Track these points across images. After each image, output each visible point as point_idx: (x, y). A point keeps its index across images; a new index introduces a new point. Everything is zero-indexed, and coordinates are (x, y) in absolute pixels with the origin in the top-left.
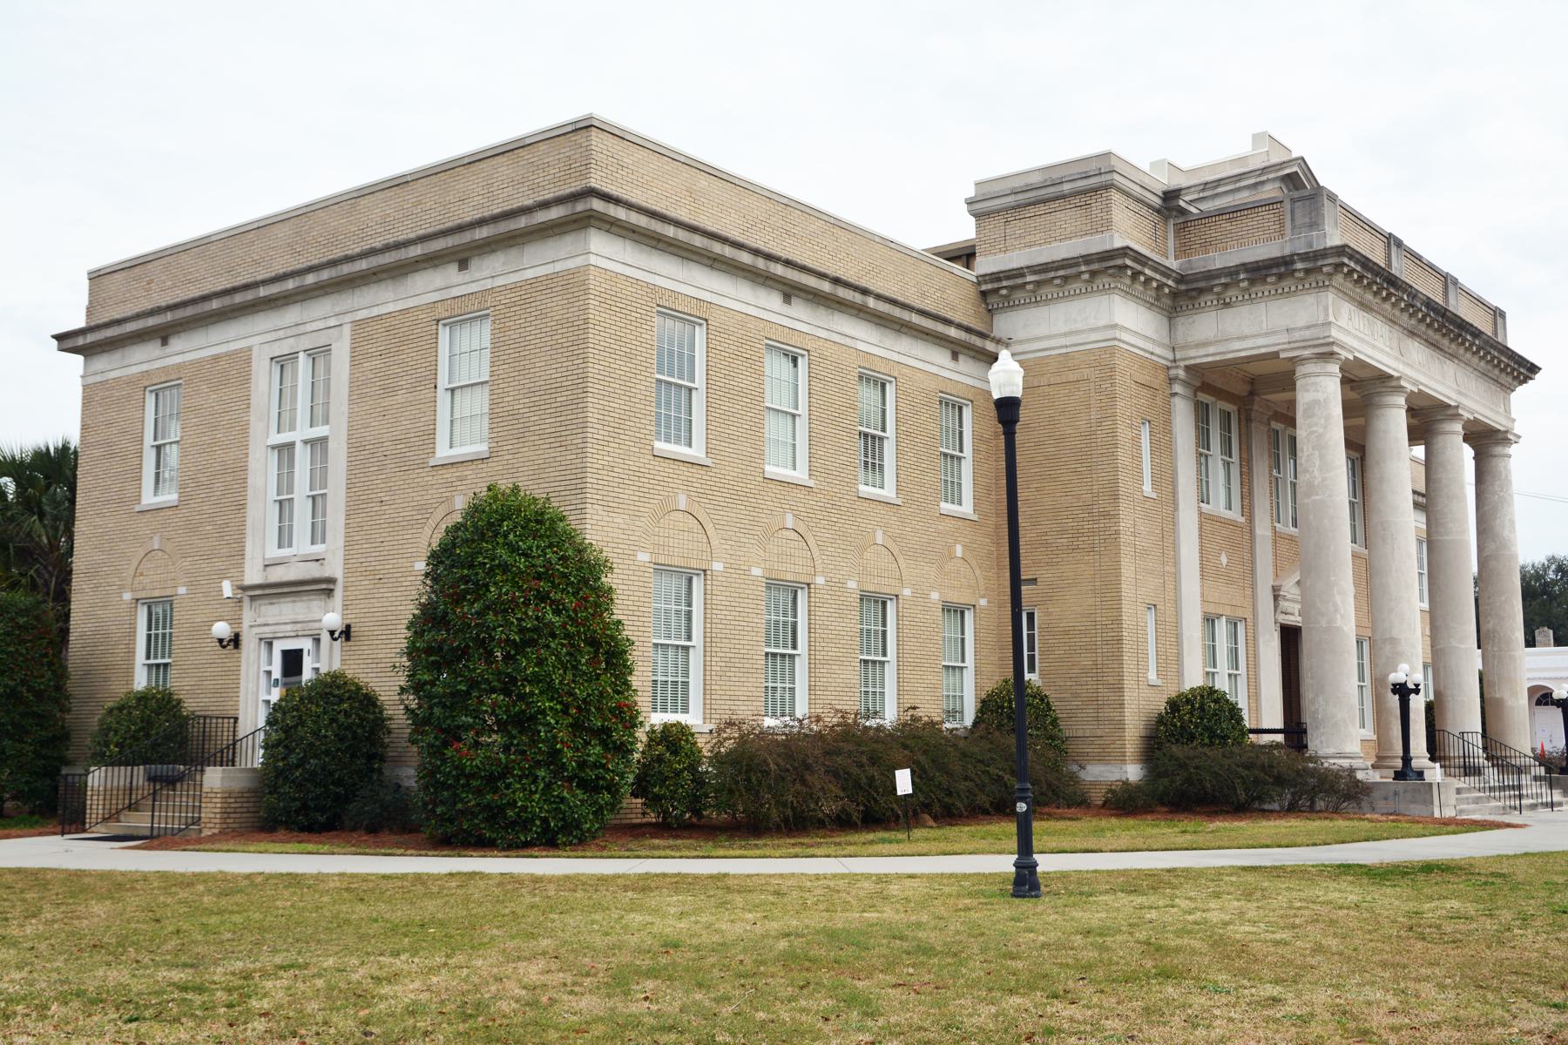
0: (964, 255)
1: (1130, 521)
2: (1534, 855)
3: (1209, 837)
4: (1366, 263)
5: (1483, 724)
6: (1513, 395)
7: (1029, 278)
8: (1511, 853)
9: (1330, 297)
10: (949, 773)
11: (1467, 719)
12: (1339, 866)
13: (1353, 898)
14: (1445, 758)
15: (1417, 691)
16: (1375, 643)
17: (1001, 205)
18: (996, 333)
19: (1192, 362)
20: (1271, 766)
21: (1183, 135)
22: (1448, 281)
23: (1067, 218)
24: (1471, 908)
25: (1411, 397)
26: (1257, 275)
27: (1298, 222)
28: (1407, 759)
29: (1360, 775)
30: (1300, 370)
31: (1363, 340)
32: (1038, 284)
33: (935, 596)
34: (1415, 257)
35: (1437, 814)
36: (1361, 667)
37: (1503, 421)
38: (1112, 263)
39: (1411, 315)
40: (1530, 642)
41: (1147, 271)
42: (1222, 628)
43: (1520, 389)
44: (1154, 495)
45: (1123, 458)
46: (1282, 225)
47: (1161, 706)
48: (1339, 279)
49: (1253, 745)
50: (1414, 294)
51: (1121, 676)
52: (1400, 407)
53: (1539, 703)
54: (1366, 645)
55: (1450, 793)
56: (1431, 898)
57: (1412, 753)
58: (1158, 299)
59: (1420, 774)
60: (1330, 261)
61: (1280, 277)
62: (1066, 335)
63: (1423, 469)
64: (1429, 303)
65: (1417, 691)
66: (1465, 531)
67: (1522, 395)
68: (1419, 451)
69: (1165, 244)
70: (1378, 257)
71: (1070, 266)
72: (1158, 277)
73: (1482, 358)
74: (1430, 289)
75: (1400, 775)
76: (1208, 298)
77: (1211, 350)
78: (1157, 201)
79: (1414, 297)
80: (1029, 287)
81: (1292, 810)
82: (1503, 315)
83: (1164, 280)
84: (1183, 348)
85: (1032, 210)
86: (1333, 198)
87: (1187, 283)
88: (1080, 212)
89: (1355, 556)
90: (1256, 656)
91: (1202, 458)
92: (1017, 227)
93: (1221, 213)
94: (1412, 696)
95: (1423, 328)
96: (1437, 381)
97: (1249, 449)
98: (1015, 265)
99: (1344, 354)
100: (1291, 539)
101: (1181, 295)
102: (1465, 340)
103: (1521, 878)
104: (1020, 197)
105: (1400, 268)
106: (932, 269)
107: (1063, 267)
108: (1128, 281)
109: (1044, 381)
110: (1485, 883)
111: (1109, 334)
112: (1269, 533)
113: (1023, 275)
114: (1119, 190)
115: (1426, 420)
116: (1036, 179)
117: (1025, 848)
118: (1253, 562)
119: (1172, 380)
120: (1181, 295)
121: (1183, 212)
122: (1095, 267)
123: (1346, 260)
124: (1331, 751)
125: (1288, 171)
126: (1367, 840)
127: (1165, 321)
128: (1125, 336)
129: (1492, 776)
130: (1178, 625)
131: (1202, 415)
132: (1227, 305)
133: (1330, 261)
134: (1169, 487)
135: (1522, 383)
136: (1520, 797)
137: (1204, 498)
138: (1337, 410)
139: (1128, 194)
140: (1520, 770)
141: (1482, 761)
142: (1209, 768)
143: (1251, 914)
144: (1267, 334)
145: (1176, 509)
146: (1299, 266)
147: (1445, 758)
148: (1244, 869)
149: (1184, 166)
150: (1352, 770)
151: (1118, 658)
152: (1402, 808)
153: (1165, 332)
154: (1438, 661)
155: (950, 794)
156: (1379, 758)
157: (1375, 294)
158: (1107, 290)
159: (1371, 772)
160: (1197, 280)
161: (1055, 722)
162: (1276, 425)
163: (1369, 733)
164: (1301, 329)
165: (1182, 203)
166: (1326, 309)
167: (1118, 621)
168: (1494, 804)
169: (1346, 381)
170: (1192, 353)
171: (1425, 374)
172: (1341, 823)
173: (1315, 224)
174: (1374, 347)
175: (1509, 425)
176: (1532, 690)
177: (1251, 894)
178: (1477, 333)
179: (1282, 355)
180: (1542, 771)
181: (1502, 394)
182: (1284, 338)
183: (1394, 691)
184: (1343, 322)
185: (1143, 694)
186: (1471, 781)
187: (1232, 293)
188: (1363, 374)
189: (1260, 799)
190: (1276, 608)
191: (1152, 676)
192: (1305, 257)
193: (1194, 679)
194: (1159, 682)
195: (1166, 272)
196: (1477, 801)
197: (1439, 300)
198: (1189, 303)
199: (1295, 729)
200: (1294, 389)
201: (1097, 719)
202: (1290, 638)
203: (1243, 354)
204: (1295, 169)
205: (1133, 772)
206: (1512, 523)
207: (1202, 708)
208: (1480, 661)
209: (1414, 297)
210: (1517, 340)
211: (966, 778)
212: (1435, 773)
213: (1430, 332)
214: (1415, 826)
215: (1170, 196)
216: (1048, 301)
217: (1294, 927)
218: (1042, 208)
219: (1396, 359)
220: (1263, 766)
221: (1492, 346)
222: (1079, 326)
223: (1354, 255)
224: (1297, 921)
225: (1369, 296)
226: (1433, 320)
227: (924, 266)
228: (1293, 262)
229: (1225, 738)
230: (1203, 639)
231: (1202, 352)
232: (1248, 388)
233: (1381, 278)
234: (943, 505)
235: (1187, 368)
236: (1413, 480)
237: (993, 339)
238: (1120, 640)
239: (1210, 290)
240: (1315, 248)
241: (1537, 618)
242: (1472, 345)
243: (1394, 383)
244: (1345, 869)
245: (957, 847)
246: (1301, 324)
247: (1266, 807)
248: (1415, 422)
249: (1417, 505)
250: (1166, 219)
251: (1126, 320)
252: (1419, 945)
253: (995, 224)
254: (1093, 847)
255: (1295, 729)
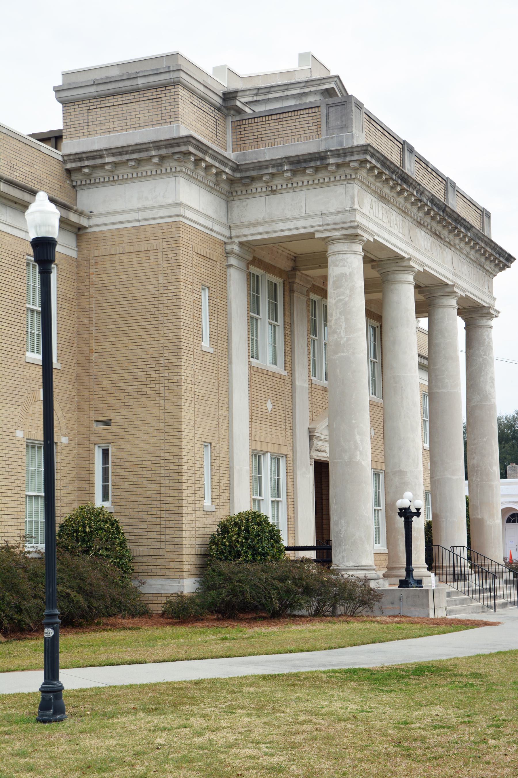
0: (54, 139)
1: (189, 371)
2: (505, 653)
3: (244, 643)
4: (384, 161)
5: (469, 538)
6: (495, 279)
7: (108, 160)
8: (486, 652)
9: (356, 188)
10: (18, 592)
11: (455, 536)
12: (347, 671)
13: (353, 707)
14: (439, 567)
15: (418, 514)
16: (387, 474)
17: (81, 94)
18: (79, 206)
19: (245, 239)
20: (301, 579)
21: (242, 47)
22: (448, 184)
23: (141, 109)
24: (452, 715)
25: (418, 275)
26: (298, 167)
27: (332, 124)
28: (409, 570)
29: (373, 584)
30: (332, 248)
31: (381, 227)
32: (116, 165)
33: (20, 434)
34: (424, 163)
35: (432, 616)
36: (377, 495)
37: (487, 299)
38: (177, 149)
39: (419, 208)
40: (504, 475)
41: (208, 159)
42: (267, 462)
43: (499, 274)
44: (211, 350)
45: (185, 317)
46: (319, 127)
47: (214, 529)
48: (363, 173)
49: (288, 561)
50: (422, 192)
51: (180, 503)
52: (409, 283)
53: (509, 521)
54: (382, 477)
55: (442, 597)
56: (420, 705)
57: (414, 564)
58: (217, 184)
59: (419, 583)
60: (356, 157)
61: (317, 169)
62: (139, 210)
63: (426, 338)
64: (433, 200)
65: (418, 514)
66: (457, 385)
67: (502, 280)
68: (424, 323)
69: (225, 138)
70: (395, 157)
71: (142, 150)
72: (217, 164)
73: (472, 248)
74: (435, 189)
75: (404, 584)
76: (258, 185)
77: (260, 229)
78: (218, 101)
79: (422, 193)
80: (107, 167)
81: (318, 614)
82: (488, 215)
83: (222, 168)
84: (238, 227)
85: (111, 101)
86: (359, 106)
87: (241, 171)
88: (151, 104)
89: (372, 404)
90: (294, 486)
91: (253, 323)
92: (99, 115)
93: (270, 114)
94: (415, 518)
95: (428, 220)
96: (438, 264)
97: (292, 314)
98: (96, 147)
99: (366, 236)
100: (324, 390)
101: (237, 181)
102: (460, 232)
103: (494, 678)
104: (102, 88)
105: (410, 168)
106: (20, 145)
107: (137, 151)
108: (191, 166)
109: (119, 250)
110: (466, 685)
111: (175, 211)
112: (306, 385)
113: (102, 157)
114: (185, 87)
115: (429, 296)
116: (115, 73)
117: (52, 671)
118: (293, 409)
119: (228, 254)
120: (237, 181)
121: (239, 111)
122: (163, 152)
123: (369, 158)
124: (351, 564)
125: (326, 86)
126: (374, 642)
127: (223, 204)
128: (188, 214)
129: (474, 581)
130: (230, 459)
131: (253, 283)
132: (274, 192)
133: (356, 157)
134: (224, 342)
135: (503, 269)
136: (495, 597)
137: (254, 354)
138: (360, 284)
139: (193, 92)
140: (494, 576)
141: (467, 569)
142: (254, 582)
143: (257, 734)
144: (305, 218)
145: (230, 362)
146: (332, 160)
147: (439, 567)
148: (264, 678)
149: (242, 73)
150: (366, 580)
151: (178, 488)
152: (405, 611)
153: (223, 213)
154: (435, 491)
155: (20, 611)
156: (389, 569)
157: (392, 188)
158: (174, 173)
159: (381, 581)
160: (250, 170)
161: (122, 544)
162: (314, 297)
163: (382, 548)
164: (332, 214)
165: (238, 104)
166: (353, 198)
167: (178, 456)
168: (476, 604)
169: (368, 260)
170: (245, 231)
171: (429, 258)
172: (356, 625)
173: (345, 127)
174: (390, 232)
175: (491, 302)
176: (504, 511)
177: (261, 708)
178: (469, 227)
179: (317, 236)
180: (510, 576)
181: (487, 278)
182: (318, 221)
183: (400, 515)
184: (366, 210)
185: (198, 520)
186: (459, 585)
187: (278, 181)
188: (381, 255)
189: (291, 606)
190: (311, 446)
191: (207, 503)
192: (336, 153)
193: (242, 505)
194: (213, 508)
195: (224, 161)
196: (463, 602)
197: (441, 197)
198: (243, 188)
199: (324, 547)
200: (326, 267)
201: (160, 540)
202: (321, 470)
203: (286, 233)
204: (332, 85)
205: (189, 586)
206: (493, 380)
207: (247, 530)
208: (467, 489)
209: (422, 193)
210: (498, 237)
211: (35, 597)
212: (431, 581)
213: (434, 224)
214: (415, 626)
215: (229, 97)
216: (124, 181)
217: (293, 746)
218: (119, 100)
219: (407, 244)
220: (294, 579)
221: (480, 238)
222: (150, 203)
223: (375, 154)
224: (298, 739)
225: (387, 190)
226: (436, 214)
227: (14, 142)
228: (326, 158)
229: (265, 555)
230: (251, 471)
231: (253, 230)
232: (291, 264)
233: (397, 175)
234: (29, 354)
235: (241, 244)
236: (419, 347)
237: (76, 211)
238: (179, 473)
239: (259, 178)
240: (345, 146)
241: (509, 457)
242: (465, 236)
243: (405, 264)
244: (352, 674)
245: (17, 662)
246: (332, 210)
247: (297, 613)
248: (421, 297)
249: (421, 367)
250: (226, 116)
251: (190, 200)
252: (405, 763)
253: (80, 110)
254: (139, 658)
255: (324, 547)
